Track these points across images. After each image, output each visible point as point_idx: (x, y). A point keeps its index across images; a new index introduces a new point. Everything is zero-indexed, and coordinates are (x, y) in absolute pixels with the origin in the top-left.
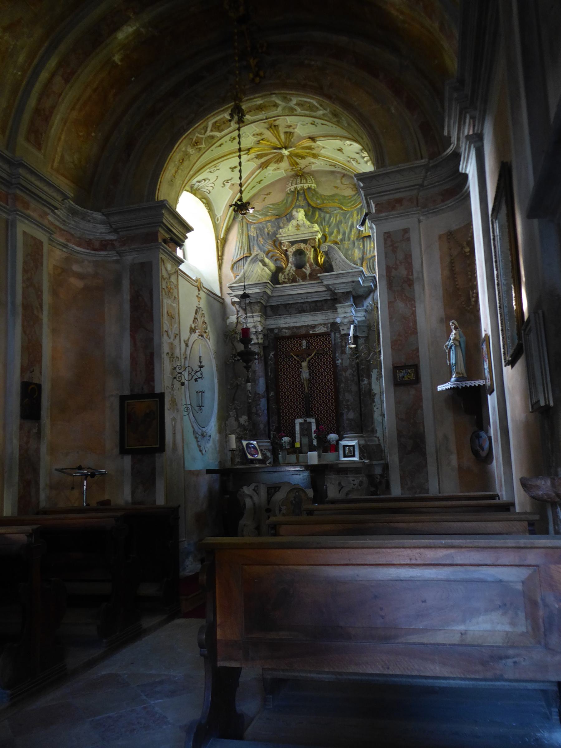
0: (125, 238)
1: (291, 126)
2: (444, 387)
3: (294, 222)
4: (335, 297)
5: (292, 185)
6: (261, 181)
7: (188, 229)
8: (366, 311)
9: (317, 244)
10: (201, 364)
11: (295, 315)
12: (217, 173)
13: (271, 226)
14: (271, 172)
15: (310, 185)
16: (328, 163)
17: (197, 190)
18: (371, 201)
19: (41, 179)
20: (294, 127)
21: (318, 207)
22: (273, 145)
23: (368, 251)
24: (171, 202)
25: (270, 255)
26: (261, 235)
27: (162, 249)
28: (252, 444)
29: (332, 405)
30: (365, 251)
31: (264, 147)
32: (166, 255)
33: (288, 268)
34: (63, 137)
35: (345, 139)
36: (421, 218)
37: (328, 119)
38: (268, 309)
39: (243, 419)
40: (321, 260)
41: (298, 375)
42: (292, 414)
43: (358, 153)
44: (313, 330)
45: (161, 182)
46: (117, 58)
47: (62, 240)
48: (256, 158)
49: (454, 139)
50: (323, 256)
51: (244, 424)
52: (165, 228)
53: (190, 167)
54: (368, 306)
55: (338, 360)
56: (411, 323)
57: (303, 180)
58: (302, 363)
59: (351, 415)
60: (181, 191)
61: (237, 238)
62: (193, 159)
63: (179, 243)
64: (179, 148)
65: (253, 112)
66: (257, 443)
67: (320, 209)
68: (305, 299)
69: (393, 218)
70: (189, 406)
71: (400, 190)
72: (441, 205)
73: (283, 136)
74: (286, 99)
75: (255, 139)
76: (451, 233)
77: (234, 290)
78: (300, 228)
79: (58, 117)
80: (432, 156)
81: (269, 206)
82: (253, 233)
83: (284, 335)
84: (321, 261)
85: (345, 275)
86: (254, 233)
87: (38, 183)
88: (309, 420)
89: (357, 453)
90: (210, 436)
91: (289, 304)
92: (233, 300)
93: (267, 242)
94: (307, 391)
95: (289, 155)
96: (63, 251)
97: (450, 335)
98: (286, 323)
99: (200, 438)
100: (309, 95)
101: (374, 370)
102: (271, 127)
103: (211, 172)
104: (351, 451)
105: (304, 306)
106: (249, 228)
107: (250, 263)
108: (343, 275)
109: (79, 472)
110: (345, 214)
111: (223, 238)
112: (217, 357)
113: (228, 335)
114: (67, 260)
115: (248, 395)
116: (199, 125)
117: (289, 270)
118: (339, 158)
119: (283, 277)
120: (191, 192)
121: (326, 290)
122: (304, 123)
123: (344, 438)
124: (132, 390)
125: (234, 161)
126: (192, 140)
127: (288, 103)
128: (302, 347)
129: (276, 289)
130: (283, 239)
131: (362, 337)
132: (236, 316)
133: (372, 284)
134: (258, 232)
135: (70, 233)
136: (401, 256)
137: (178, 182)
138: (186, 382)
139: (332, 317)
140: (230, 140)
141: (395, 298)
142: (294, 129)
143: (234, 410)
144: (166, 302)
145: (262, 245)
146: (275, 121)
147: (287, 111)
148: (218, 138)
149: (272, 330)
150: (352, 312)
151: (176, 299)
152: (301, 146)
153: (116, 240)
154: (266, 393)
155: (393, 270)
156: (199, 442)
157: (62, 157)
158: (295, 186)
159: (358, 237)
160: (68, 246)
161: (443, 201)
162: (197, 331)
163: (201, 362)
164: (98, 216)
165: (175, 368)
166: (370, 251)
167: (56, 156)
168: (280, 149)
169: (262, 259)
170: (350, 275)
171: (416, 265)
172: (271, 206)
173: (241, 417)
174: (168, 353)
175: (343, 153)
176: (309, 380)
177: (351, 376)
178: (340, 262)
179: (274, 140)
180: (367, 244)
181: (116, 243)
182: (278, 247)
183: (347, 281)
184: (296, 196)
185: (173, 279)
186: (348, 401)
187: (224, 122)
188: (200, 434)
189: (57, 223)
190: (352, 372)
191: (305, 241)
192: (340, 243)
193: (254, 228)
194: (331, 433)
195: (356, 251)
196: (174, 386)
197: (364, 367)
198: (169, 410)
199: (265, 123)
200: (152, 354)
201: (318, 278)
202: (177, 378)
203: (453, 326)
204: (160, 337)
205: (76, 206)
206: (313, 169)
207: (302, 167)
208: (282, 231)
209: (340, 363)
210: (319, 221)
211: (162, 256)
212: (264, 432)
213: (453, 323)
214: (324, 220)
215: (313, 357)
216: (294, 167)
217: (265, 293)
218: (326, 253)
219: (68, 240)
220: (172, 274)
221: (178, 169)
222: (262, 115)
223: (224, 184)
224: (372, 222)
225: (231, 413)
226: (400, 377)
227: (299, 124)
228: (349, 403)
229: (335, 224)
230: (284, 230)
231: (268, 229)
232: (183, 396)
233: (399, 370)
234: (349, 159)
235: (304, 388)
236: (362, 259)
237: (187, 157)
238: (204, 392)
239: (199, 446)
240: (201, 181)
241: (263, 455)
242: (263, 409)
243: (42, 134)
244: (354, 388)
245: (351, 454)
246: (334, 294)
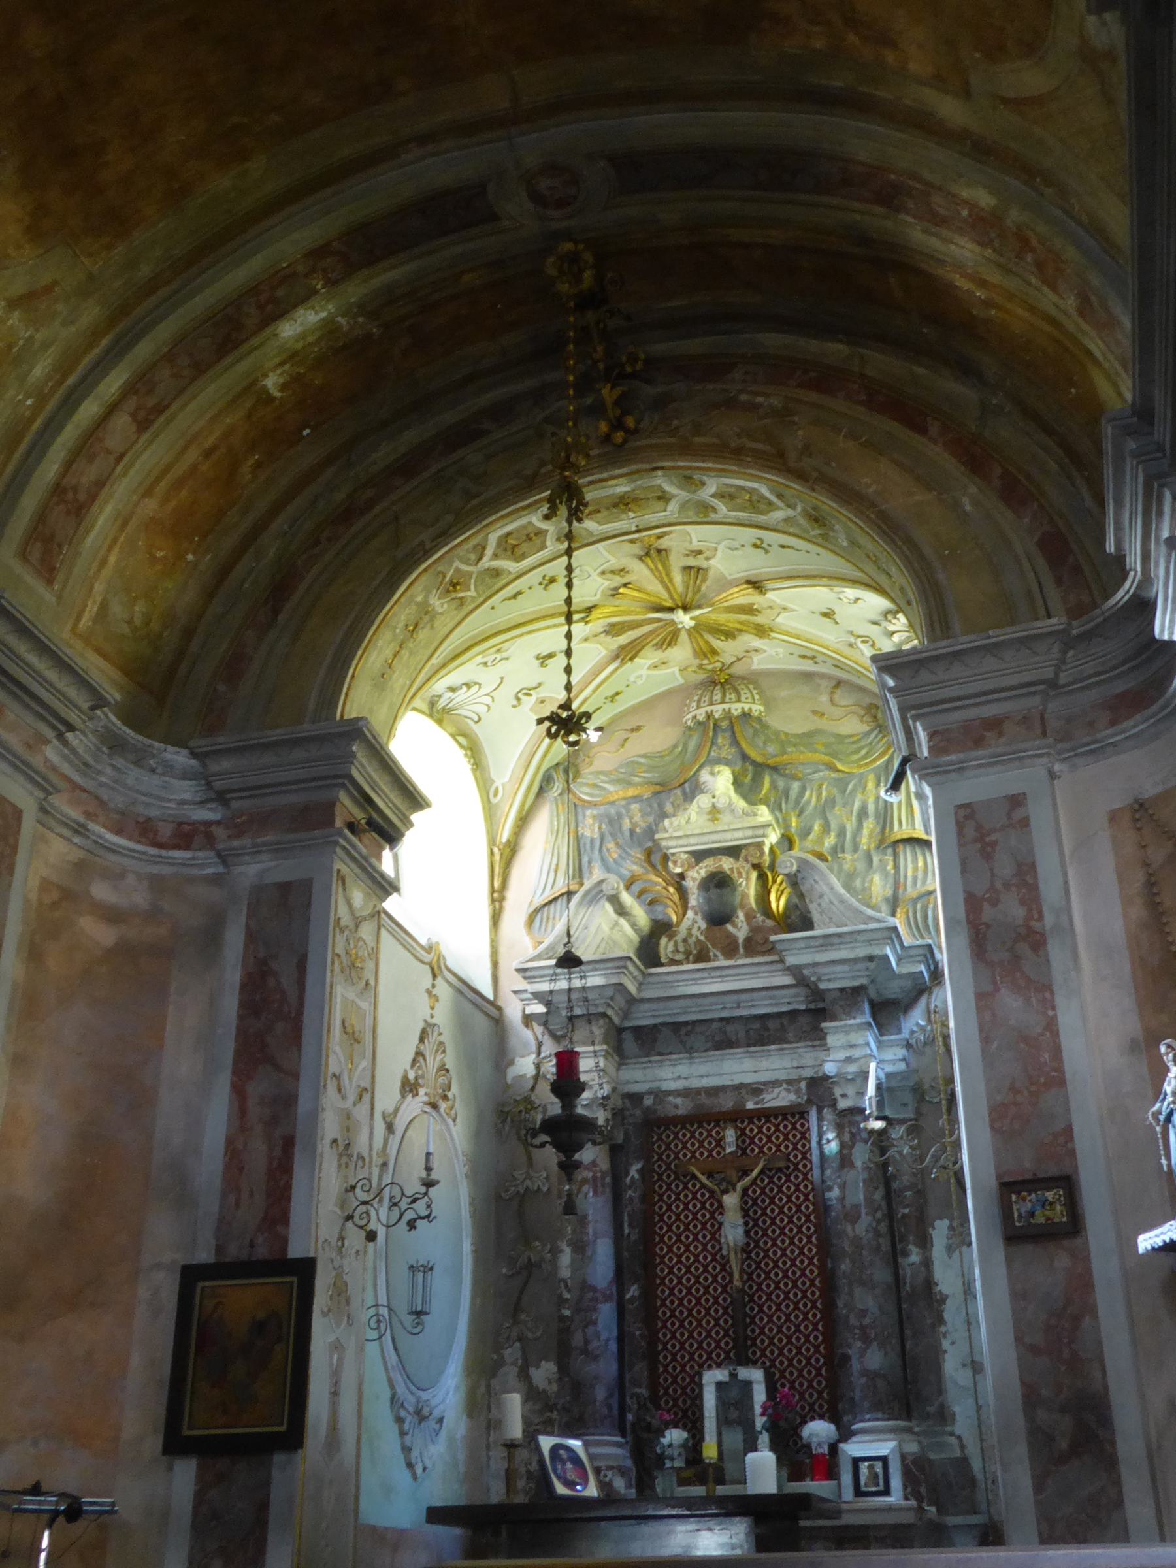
0: (244, 818)
1: (700, 552)
2: (1157, 1236)
3: (703, 801)
4: (820, 1005)
5: (698, 707)
6: (617, 694)
7: (415, 800)
8: (908, 1045)
9: (767, 859)
10: (428, 1175)
11: (704, 1054)
12: (502, 668)
13: (641, 811)
14: (645, 672)
15: (747, 707)
16: (798, 651)
17: (446, 711)
18: (918, 724)
19: (44, 649)
20: (707, 554)
21: (770, 762)
22: (653, 599)
23: (909, 880)
24: (377, 721)
25: (636, 888)
26: (611, 834)
27: (344, 848)
28: (568, 1449)
29: (817, 1351)
30: (902, 880)
31: (628, 607)
32: (353, 865)
33: (686, 923)
34: (112, 559)
35: (839, 583)
36: (1057, 767)
37: (797, 531)
38: (628, 1037)
39: (544, 1373)
40: (778, 902)
41: (713, 1235)
42: (692, 1355)
43: (875, 623)
44: (756, 1099)
45: (353, 676)
46: (272, 383)
47: (75, 814)
48: (606, 632)
49: (1134, 560)
50: (782, 892)
51: (544, 1391)
52: (355, 793)
53: (435, 644)
54: (913, 1032)
55: (830, 1189)
56: (1047, 1056)
57: (728, 696)
58: (725, 1197)
59: (875, 1359)
60: (402, 710)
61: (546, 843)
62: (442, 624)
63: (390, 836)
64: (408, 594)
65: (604, 513)
66: (586, 1445)
67: (775, 769)
68: (731, 1008)
69: (980, 766)
70: (384, 1311)
71: (996, 696)
72: (1109, 731)
73: (678, 578)
74: (689, 481)
75: (607, 583)
76: (1141, 805)
77: (535, 977)
78: (718, 816)
79: (109, 509)
80: (1076, 612)
81: (636, 759)
82: (590, 828)
83: (672, 1112)
84: (778, 907)
85: (848, 939)
86: (593, 831)
87: (33, 659)
88: (744, 1373)
89: (896, 1483)
90: (440, 1421)
91: (686, 1023)
92: (528, 1011)
93: (629, 855)
94: (737, 1283)
95: (693, 628)
96: (71, 842)
97: (1164, 1080)
98: (679, 1078)
99: (409, 1421)
100: (748, 471)
101: (938, 1223)
102: (648, 554)
103: (485, 664)
104: (876, 1476)
105: (730, 1028)
106: (580, 818)
107: (580, 904)
108: (841, 940)
109: (31, 1502)
110: (841, 784)
111: (508, 841)
112: (474, 1176)
113: (508, 1112)
114: (81, 868)
115: (561, 1295)
116: (465, 541)
117: (689, 929)
118: (825, 635)
119: (671, 947)
120: (431, 716)
121: (794, 982)
122: (736, 544)
123: (853, 1434)
124: (220, 1249)
125: (552, 638)
126: (444, 577)
127: (694, 492)
128: (724, 1149)
129: (651, 979)
130: (671, 843)
131: (902, 1122)
132: (534, 1056)
133: (923, 968)
134: (604, 826)
135: (97, 797)
136: (1005, 868)
137: (398, 680)
138: (381, 1232)
139: (810, 1062)
140: (540, 584)
141: (994, 983)
142: (708, 559)
143: (518, 1344)
144: (342, 994)
145: (615, 861)
146: (659, 537)
147: (691, 513)
148: (511, 577)
149: (635, 1098)
150: (868, 1044)
151: (369, 988)
152: (725, 604)
153: (218, 823)
154: (614, 1288)
155: (986, 905)
156: (407, 1434)
157: (104, 607)
158: (709, 709)
159: (881, 841)
160: (88, 830)
161: (1113, 723)
162: (422, 1091)
163: (429, 1169)
164: (180, 758)
165: (353, 1188)
166: (915, 879)
167: (90, 603)
168: (671, 610)
169: (614, 892)
170: (859, 938)
171: (1050, 892)
172: (642, 760)
173: (538, 1367)
174: (335, 1141)
175: (837, 623)
176: (746, 1250)
177: (870, 1235)
178: (831, 902)
179: (656, 588)
180: (906, 860)
181: (220, 832)
182: (659, 867)
183: (851, 955)
184: (711, 734)
185: (366, 931)
186: (863, 1313)
187: (528, 535)
188: (411, 1409)
189: (66, 769)
190: (874, 1224)
191: (733, 852)
192: (830, 858)
193: (594, 817)
194: (813, 1419)
195: (877, 879)
196: (346, 1242)
197: (907, 1211)
198: (325, 1314)
199: (632, 541)
200: (289, 1143)
201: (771, 949)
202: (356, 1219)
203: (1171, 1055)
204: (318, 1091)
205: (124, 728)
206: (755, 666)
207: (728, 660)
208: (671, 824)
209: (837, 1199)
210: (772, 800)
211: (341, 865)
212: (605, 1411)
213: (1169, 1046)
214: (787, 797)
215: (756, 1179)
216: (706, 662)
217: (620, 987)
218: (794, 881)
219: (88, 815)
220: (364, 919)
221: (401, 647)
222: (626, 522)
223: (518, 699)
224: (921, 778)
225: (507, 1353)
226: (1020, 1215)
227: (721, 547)
228: (867, 1321)
229: (816, 807)
230: (676, 821)
231: (631, 818)
232: (369, 1277)
233: (1018, 1193)
234: (852, 639)
235: (731, 1274)
236: (894, 904)
237: (427, 618)
238: (431, 1269)
239: (406, 1450)
240: (460, 688)
241: (603, 1485)
242: (604, 1336)
243: (60, 546)
244: (881, 1274)
245: (877, 1485)
246: (816, 994)
